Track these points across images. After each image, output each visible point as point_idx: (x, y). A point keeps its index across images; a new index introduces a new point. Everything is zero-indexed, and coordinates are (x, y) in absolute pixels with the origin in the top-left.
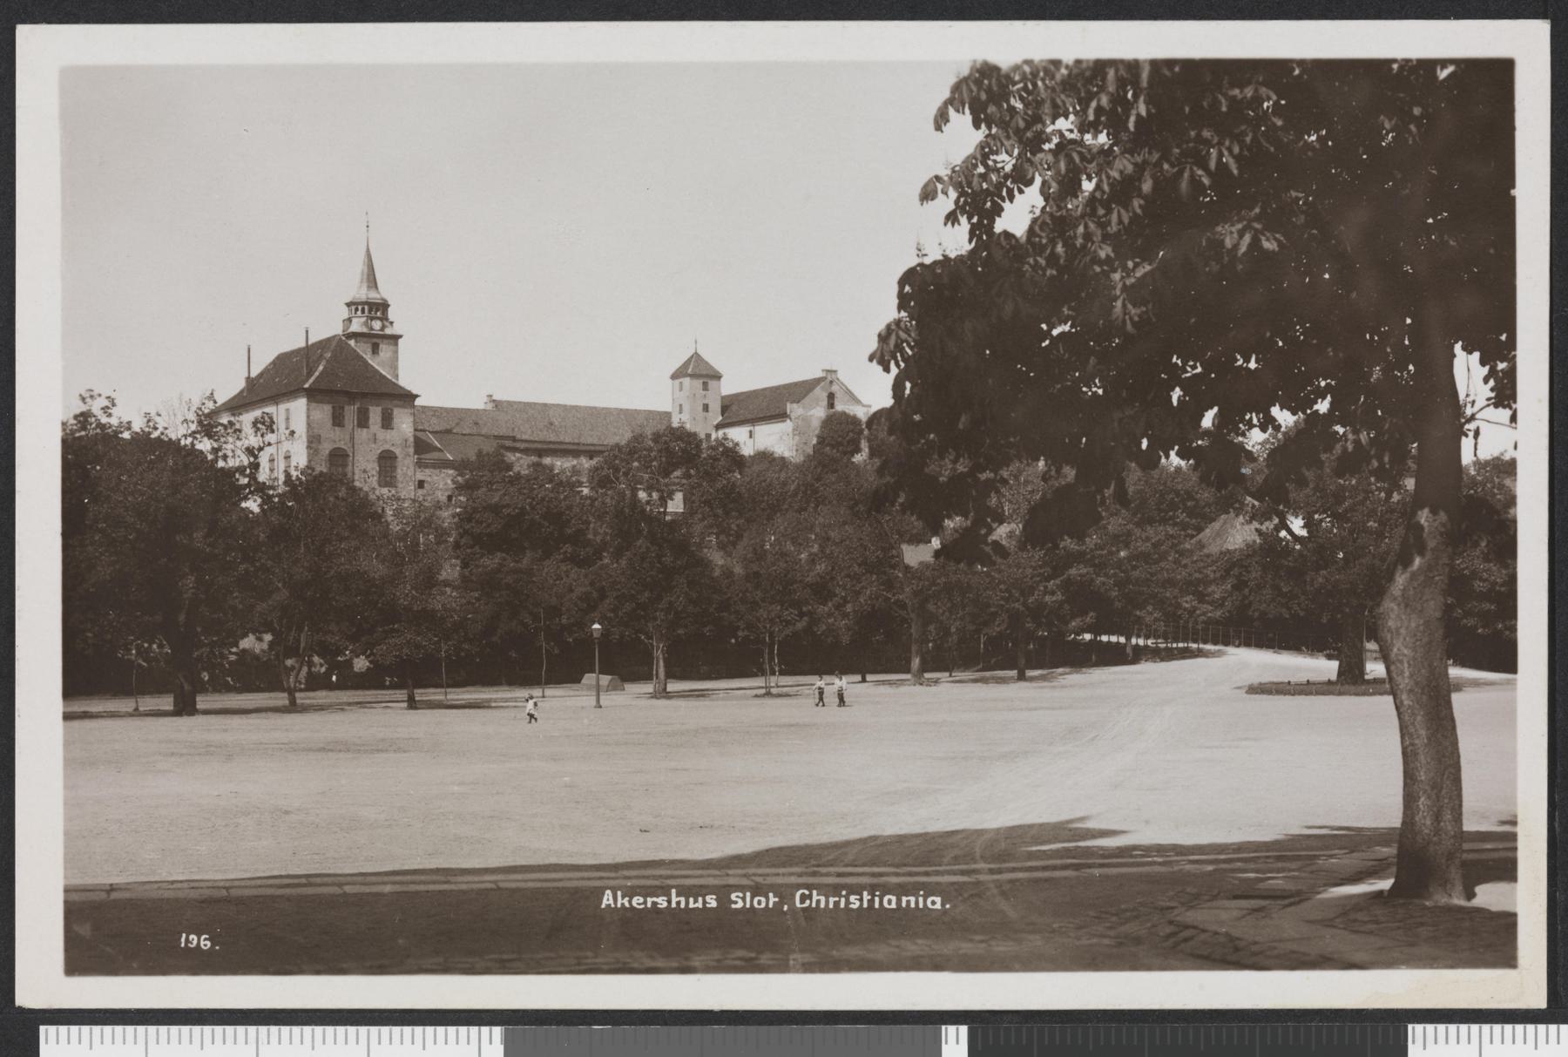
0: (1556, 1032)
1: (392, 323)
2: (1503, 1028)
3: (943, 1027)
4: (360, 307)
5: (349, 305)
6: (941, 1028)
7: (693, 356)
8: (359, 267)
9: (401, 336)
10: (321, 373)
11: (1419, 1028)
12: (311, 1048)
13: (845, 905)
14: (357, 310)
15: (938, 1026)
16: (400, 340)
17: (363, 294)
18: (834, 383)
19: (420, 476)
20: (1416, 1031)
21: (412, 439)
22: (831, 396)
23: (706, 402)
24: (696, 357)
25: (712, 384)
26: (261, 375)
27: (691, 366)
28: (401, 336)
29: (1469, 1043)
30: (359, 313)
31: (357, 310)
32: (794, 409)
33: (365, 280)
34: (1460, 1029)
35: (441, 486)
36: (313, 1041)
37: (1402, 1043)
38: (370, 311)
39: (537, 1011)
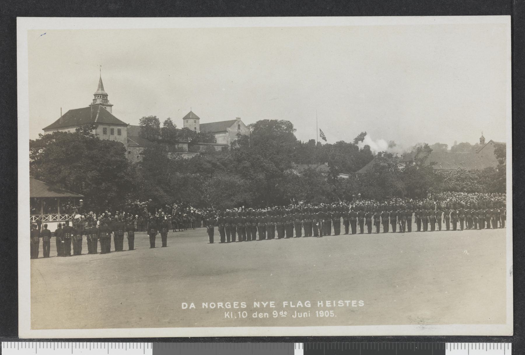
1: (109, 101)
2: (497, 344)
3: (295, 343)
4: (99, 96)
7: (190, 112)
8: (98, 82)
9: (113, 105)
10: (99, 117)
13: (333, 302)
14: (98, 97)
16: (112, 107)
17: (100, 92)
18: (240, 122)
19: (129, 150)
20: (448, 345)
21: (126, 138)
22: (239, 125)
23: (195, 127)
24: (191, 113)
25: (197, 121)
27: (191, 116)
28: (113, 105)
29: (79, 348)
30: (99, 98)
32: (229, 129)
33: (100, 87)
34: (498, 344)
35: (135, 153)
38: (103, 97)
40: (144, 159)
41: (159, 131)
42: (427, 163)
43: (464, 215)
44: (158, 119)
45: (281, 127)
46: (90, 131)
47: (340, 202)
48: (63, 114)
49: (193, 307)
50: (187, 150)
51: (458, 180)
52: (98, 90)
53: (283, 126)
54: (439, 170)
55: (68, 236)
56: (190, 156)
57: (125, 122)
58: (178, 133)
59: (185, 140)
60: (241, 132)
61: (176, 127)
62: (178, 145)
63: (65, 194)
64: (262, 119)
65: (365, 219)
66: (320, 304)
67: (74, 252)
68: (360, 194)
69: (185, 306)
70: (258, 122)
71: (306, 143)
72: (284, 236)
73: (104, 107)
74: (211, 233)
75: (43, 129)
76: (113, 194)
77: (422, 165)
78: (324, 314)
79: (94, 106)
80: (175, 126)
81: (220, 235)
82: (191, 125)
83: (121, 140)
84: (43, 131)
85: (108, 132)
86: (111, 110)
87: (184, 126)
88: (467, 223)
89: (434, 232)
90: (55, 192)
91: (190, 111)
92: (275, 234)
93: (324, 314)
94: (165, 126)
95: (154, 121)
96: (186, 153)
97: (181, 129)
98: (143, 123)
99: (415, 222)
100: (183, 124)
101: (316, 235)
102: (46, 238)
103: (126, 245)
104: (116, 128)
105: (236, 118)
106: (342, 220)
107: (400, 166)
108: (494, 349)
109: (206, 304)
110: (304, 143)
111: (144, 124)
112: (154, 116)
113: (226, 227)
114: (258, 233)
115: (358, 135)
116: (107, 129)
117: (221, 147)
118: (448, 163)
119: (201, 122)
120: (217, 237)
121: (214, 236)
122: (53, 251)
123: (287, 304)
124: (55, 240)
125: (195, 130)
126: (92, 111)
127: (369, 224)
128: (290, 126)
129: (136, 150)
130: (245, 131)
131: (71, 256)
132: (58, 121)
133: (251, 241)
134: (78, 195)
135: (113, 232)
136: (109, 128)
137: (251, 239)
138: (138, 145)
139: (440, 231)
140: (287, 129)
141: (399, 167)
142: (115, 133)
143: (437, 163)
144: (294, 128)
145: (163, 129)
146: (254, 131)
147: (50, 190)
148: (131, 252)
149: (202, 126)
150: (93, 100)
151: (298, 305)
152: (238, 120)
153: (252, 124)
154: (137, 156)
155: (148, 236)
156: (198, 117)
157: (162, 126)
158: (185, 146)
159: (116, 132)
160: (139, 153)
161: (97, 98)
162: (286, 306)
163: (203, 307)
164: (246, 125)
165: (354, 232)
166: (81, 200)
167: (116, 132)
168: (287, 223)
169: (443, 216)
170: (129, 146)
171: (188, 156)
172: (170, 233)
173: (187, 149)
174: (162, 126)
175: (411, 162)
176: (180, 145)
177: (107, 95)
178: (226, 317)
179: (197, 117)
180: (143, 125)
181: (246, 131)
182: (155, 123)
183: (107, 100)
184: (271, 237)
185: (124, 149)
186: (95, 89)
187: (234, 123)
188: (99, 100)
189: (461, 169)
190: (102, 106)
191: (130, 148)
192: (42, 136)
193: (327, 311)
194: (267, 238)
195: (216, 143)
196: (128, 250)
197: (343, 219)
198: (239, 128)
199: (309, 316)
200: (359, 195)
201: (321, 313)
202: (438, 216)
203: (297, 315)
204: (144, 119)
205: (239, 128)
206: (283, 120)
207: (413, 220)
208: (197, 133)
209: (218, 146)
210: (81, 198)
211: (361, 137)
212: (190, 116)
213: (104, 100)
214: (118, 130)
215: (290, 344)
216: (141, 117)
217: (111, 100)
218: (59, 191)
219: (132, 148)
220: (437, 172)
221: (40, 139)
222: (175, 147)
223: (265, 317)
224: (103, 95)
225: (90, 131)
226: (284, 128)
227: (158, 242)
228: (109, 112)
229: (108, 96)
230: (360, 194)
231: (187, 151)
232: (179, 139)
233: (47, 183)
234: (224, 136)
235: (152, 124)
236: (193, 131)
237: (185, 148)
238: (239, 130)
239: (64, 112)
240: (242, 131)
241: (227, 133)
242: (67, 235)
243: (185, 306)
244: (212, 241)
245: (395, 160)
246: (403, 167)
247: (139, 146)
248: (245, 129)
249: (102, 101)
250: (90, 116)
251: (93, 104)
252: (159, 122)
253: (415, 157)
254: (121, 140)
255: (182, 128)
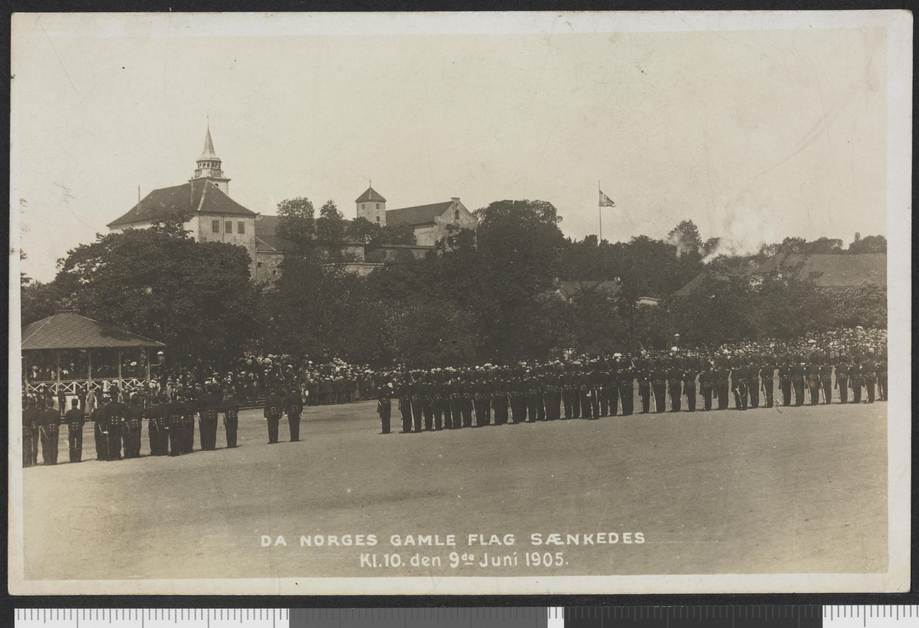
0: (207, 613)
1: (223, 172)
4: (206, 163)
5: (198, 162)
6: (822, 607)
7: (369, 190)
8: (203, 138)
9: (230, 180)
10: (204, 201)
11: (828, 607)
12: (174, 622)
14: (204, 165)
15: (545, 608)
16: (229, 182)
17: (208, 156)
19: (259, 260)
21: (254, 239)
22: (457, 212)
24: (370, 191)
25: (381, 204)
26: (147, 199)
28: (230, 180)
30: (206, 166)
31: (204, 165)
32: (438, 219)
33: (208, 148)
36: (176, 618)
37: (819, 616)
39: (893, 594)
40: (284, 275)
41: (313, 225)
42: (803, 275)
43: (875, 374)
44: (311, 202)
45: (535, 213)
46: (177, 225)
47: (642, 350)
48: (142, 198)
49: (281, 542)
50: (362, 258)
51: (862, 305)
52: (204, 153)
53: (537, 212)
54: (827, 287)
55: (115, 422)
56: (369, 269)
57: (251, 209)
58: (346, 227)
59: (360, 241)
60: (460, 223)
61: (342, 216)
62: (347, 249)
63: (131, 342)
64: (500, 200)
65: (682, 383)
66: (536, 538)
67: (125, 452)
68: (677, 335)
69: (266, 541)
70: (492, 205)
71: (579, 242)
72: (525, 418)
73: (214, 183)
74: (385, 413)
75: (108, 226)
76: (218, 340)
77: (795, 278)
78: (542, 560)
79: (198, 183)
80: (341, 216)
81: (402, 417)
82: (377, 216)
83: (244, 243)
84: (108, 228)
85: (222, 228)
86: (227, 189)
87: (358, 214)
88: (882, 387)
89: (802, 408)
90: (113, 338)
91: (369, 187)
92: (509, 413)
93: (542, 560)
94: (323, 215)
95: (303, 207)
96: (362, 263)
97: (352, 220)
98: (285, 211)
99: (780, 388)
100: (356, 210)
101: (587, 416)
102: (76, 424)
103: (221, 437)
104: (235, 221)
105: (452, 198)
106: (636, 384)
107: (752, 281)
108: (852, 616)
109: (307, 539)
110: (577, 241)
111: (286, 213)
112: (303, 198)
113: (413, 402)
114: (475, 413)
115: (676, 227)
116: (220, 222)
117: (424, 252)
118: (844, 275)
119: (389, 206)
120: (397, 421)
121: (391, 419)
122: (89, 449)
123: (475, 540)
124: (91, 432)
125: (377, 222)
126: (192, 190)
127: (691, 393)
128: (550, 211)
129: (270, 259)
130: (468, 222)
131: (120, 459)
132: (135, 209)
133: (460, 428)
134: (155, 343)
135: (198, 414)
136: (222, 221)
137: (462, 425)
138: (275, 250)
139: (828, 405)
140: (544, 216)
141: (751, 282)
142: (233, 229)
143: (822, 273)
144: (558, 214)
145: (320, 221)
146: (486, 221)
147: (104, 334)
148: (233, 451)
149: (391, 214)
150: (196, 171)
151: (492, 541)
152: (455, 202)
153: (482, 209)
154: (272, 270)
155: (266, 419)
156: (384, 199)
157: (317, 215)
158: (360, 251)
159: (235, 228)
160: (276, 265)
161: (202, 167)
162: (473, 542)
163: (302, 544)
164: (471, 211)
165: (661, 408)
166: (160, 353)
167: (235, 228)
168: (531, 392)
169: (833, 377)
170: (258, 253)
171: (365, 268)
172: (308, 412)
173: (363, 256)
174: (317, 215)
175: (774, 273)
176: (350, 250)
177: (220, 162)
178: (362, 565)
179: (382, 197)
180: (284, 215)
181: (469, 223)
182: (304, 210)
183: (219, 170)
184: (501, 419)
185: (248, 257)
186: (200, 153)
187: (448, 207)
188: (205, 170)
189: (868, 284)
190: (210, 182)
191: (260, 257)
192: (102, 238)
193: (548, 554)
194: (492, 422)
195: (415, 245)
196: (226, 448)
197: (638, 384)
198: (457, 217)
199: (516, 564)
200: (677, 336)
201: (536, 557)
202: (825, 375)
203: (490, 563)
204: (286, 204)
205: (457, 217)
206: (537, 201)
207: (776, 383)
208: (382, 226)
209: (419, 250)
210: (161, 348)
211: (857, 236)
212: (370, 197)
213: (214, 170)
214: (239, 224)
215: (539, 609)
216: (280, 201)
217: (227, 171)
218: (122, 337)
219: (263, 257)
220: (824, 291)
221: (99, 242)
222: (341, 253)
223: (433, 564)
224: (213, 162)
225: (177, 225)
226: (540, 214)
227: (284, 429)
228: (224, 192)
229: (221, 164)
230: (677, 335)
231: (364, 259)
232: (349, 238)
233: (100, 321)
234: (429, 232)
235: (299, 212)
236: (374, 223)
237: (359, 256)
238: (457, 220)
239: (144, 195)
240: (462, 221)
241: (435, 226)
242: (113, 420)
243: (266, 541)
244: (386, 429)
245: (743, 270)
246: (758, 283)
247: (275, 253)
248: (468, 217)
249: (211, 173)
250: (190, 199)
251: (194, 178)
252: (312, 208)
253: (781, 264)
254: (244, 243)
255: (354, 219)
